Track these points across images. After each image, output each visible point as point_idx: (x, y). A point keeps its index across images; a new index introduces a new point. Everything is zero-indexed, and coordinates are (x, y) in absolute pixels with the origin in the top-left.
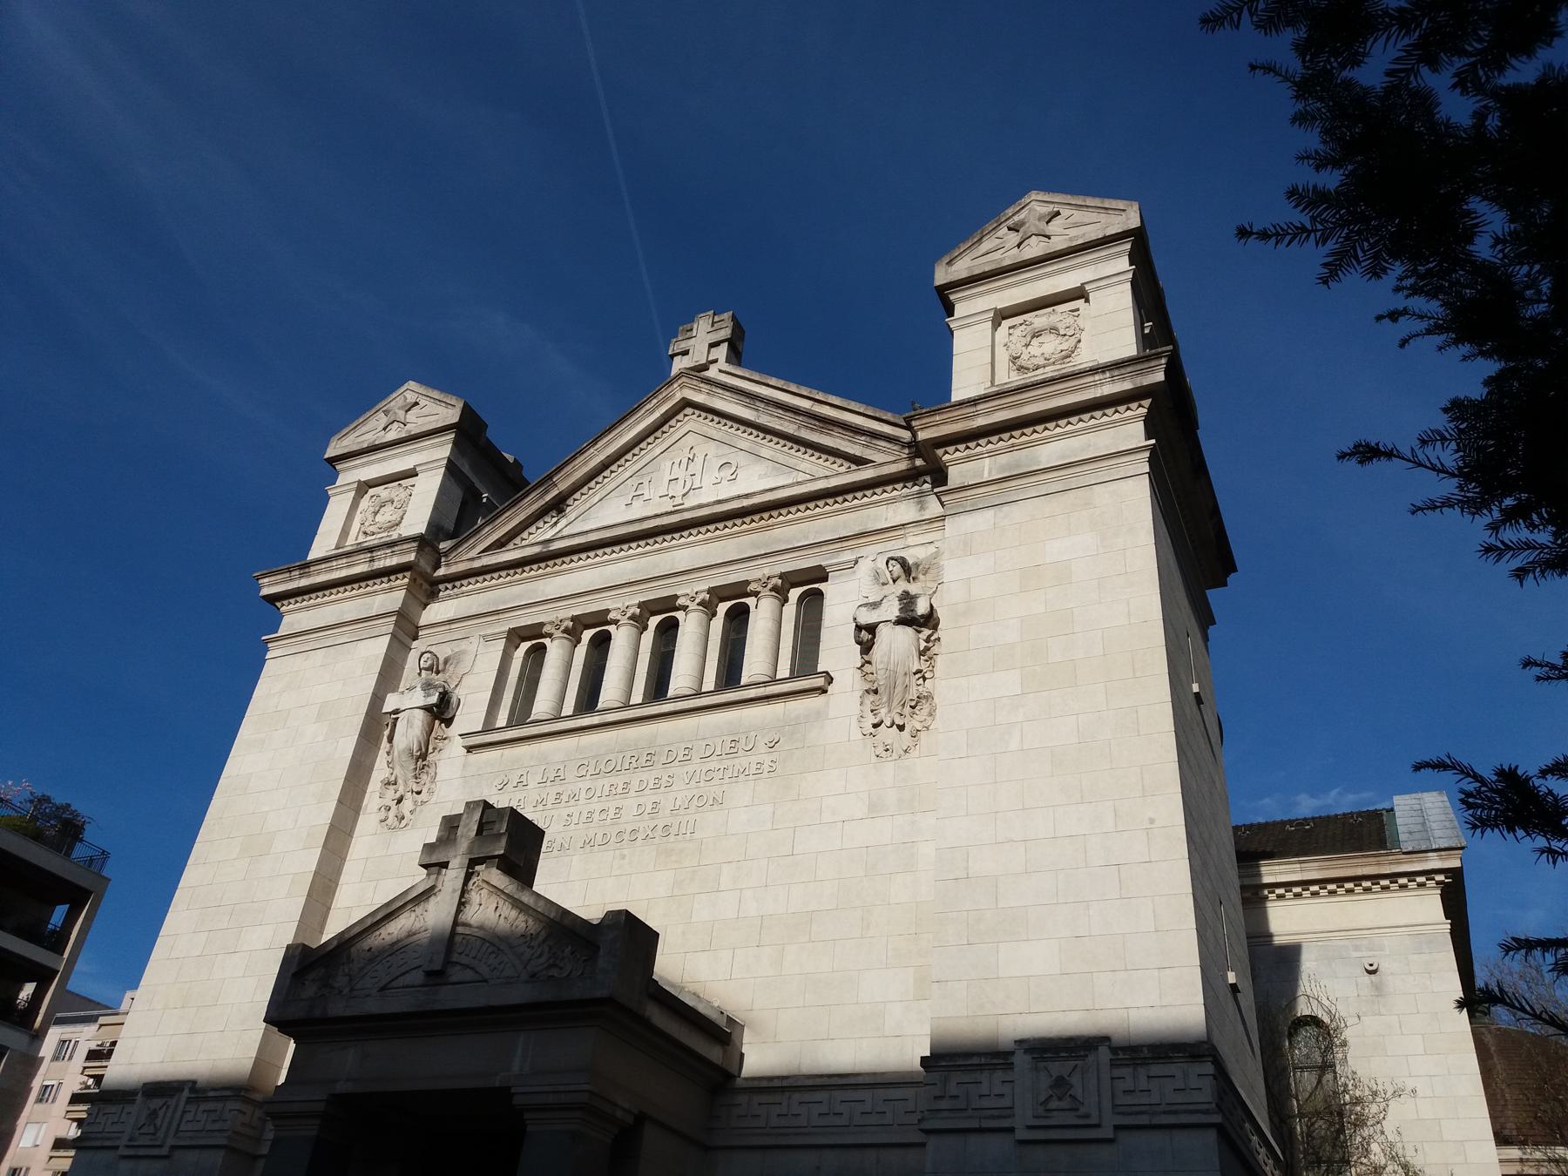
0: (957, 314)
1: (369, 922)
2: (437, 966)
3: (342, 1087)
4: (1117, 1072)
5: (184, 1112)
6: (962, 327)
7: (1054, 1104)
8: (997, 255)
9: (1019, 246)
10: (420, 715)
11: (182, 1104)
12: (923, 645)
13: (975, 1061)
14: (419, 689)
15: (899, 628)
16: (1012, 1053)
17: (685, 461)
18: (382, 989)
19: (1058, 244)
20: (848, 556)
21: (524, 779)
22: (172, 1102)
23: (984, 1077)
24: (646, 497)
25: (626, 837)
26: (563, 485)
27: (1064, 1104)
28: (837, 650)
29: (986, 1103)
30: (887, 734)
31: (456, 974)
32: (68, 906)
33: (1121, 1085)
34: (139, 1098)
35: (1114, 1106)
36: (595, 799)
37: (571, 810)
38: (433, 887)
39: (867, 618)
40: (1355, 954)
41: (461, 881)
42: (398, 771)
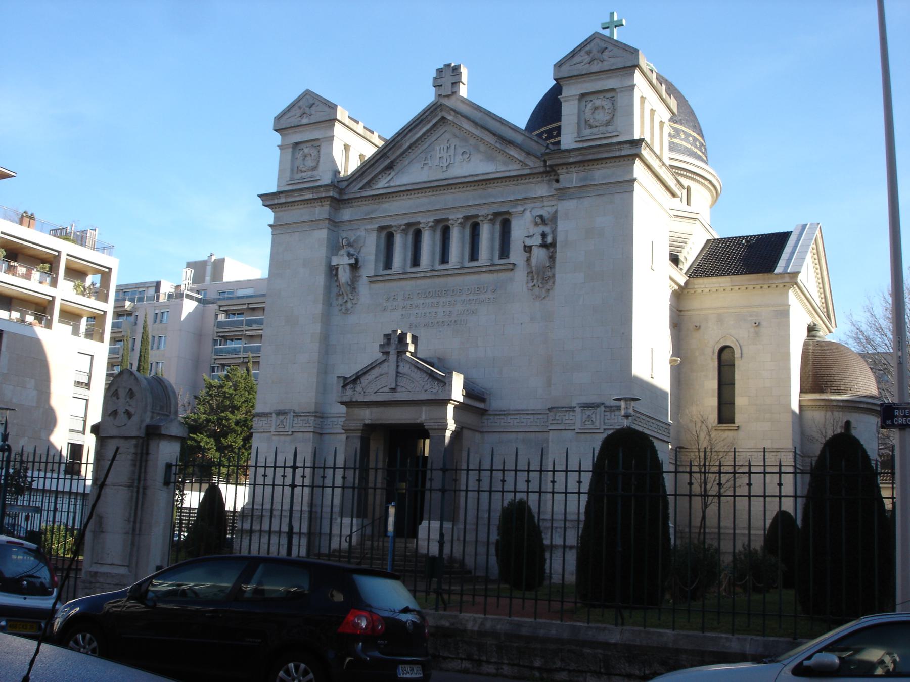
0: (564, 94)
1: (365, 370)
2: (393, 387)
3: (367, 422)
4: (606, 413)
5: (293, 420)
6: (566, 101)
7: (587, 423)
8: (580, 66)
9: (589, 63)
10: (348, 267)
11: (292, 418)
12: (550, 254)
13: (564, 409)
14: (345, 255)
15: (541, 248)
16: (575, 407)
17: (446, 147)
18: (375, 393)
19: (606, 66)
20: (520, 208)
21: (396, 297)
22: (288, 417)
23: (567, 414)
24: (430, 165)
25: (440, 323)
26: (392, 158)
27: (590, 423)
28: (516, 255)
29: (567, 422)
30: (536, 290)
31: (399, 389)
32: (891, 670)
33: (607, 417)
34: (274, 415)
35: (604, 423)
36: (426, 308)
37: (417, 311)
38: (385, 360)
39: (529, 242)
40: (751, 318)
41: (396, 358)
42: (342, 289)
